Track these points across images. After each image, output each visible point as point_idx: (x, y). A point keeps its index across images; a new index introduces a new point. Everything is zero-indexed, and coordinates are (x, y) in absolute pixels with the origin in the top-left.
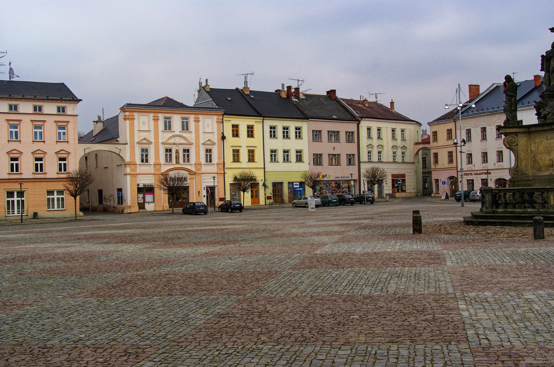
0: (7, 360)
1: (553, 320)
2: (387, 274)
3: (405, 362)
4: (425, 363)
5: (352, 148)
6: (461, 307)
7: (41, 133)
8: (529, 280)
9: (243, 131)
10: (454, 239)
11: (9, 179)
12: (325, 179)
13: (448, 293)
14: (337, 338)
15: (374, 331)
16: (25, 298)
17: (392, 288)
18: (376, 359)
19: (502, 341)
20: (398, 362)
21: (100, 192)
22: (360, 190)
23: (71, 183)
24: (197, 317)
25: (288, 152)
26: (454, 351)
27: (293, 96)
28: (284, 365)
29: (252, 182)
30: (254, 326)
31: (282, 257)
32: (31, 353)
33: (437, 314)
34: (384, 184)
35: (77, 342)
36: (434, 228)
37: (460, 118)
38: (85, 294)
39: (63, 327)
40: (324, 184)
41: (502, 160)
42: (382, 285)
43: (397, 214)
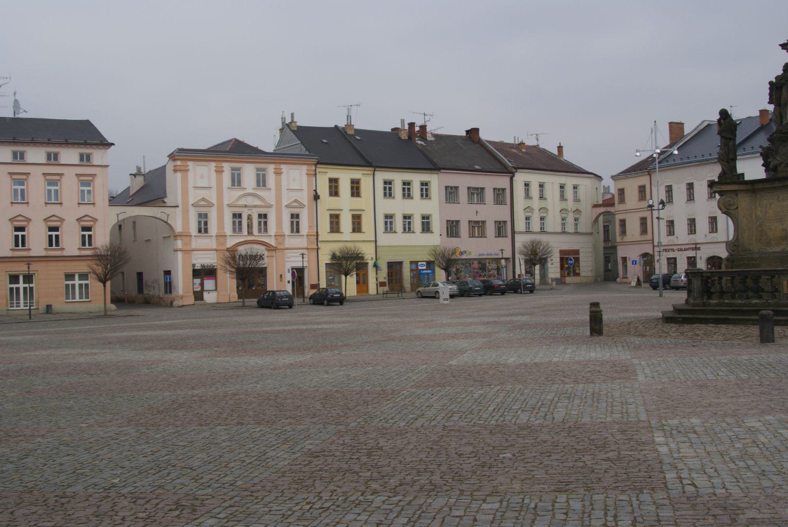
0: (12, 513)
1: (785, 457)
2: (554, 394)
3: (578, 519)
4: (606, 520)
5: (502, 213)
6: (657, 440)
7: (56, 191)
8: (753, 401)
9: (345, 187)
10: (649, 343)
11: (12, 257)
12: (464, 257)
13: (639, 421)
14: (481, 486)
15: (533, 475)
16: (36, 426)
17: (560, 414)
18: (536, 515)
19: (714, 487)
20: (568, 519)
21: (140, 275)
22: (514, 272)
23: (98, 262)
24: (278, 455)
25: (409, 218)
26: (647, 503)
27: (417, 137)
28: (404, 524)
29: (358, 261)
30: (361, 469)
31: (401, 370)
32: (44, 503)
33: (624, 450)
34: (549, 264)
35: (109, 489)
36: (621, 328)
37: (657, 169)
38: (119, 422)
39: (89, 468)
40: (463, 264)
41: (716, 230)
42: (546, 410)
43: (567, 307)
